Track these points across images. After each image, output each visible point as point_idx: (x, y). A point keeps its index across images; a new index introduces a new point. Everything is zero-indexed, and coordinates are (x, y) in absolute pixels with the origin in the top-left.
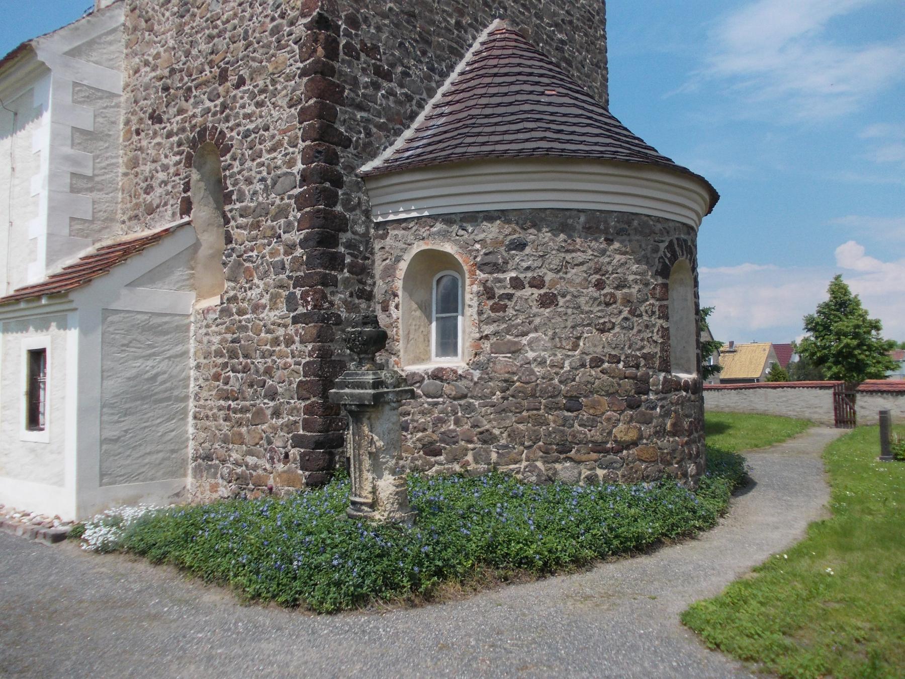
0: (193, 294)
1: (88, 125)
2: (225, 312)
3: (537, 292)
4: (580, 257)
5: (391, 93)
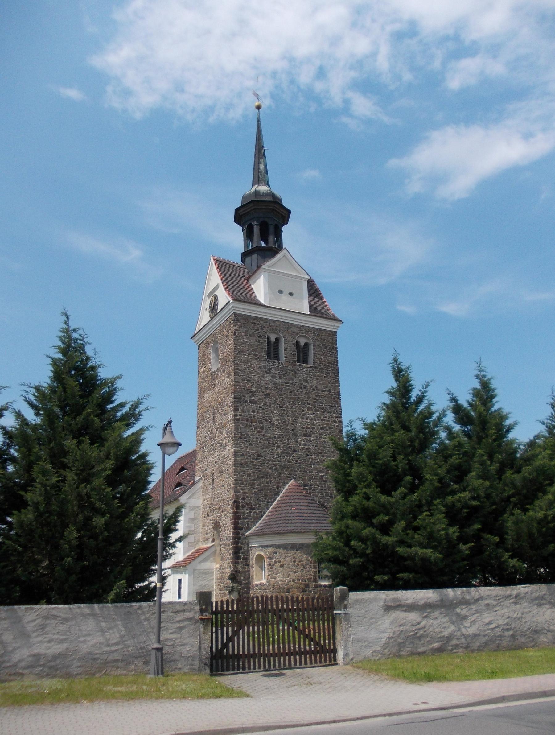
0: (215, 563)
1: (192, 516)
2: (220, 569)
3: (279, 564)
4: (289, 555)
5: (255, 512)
